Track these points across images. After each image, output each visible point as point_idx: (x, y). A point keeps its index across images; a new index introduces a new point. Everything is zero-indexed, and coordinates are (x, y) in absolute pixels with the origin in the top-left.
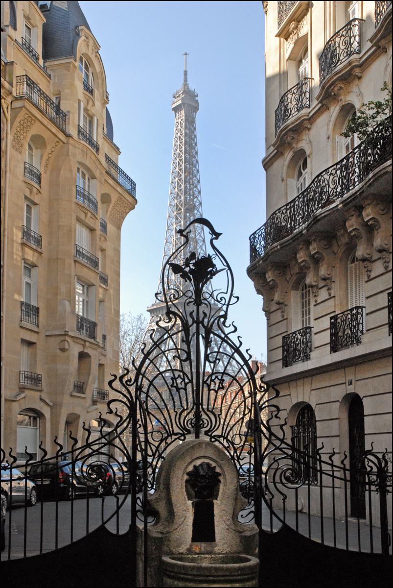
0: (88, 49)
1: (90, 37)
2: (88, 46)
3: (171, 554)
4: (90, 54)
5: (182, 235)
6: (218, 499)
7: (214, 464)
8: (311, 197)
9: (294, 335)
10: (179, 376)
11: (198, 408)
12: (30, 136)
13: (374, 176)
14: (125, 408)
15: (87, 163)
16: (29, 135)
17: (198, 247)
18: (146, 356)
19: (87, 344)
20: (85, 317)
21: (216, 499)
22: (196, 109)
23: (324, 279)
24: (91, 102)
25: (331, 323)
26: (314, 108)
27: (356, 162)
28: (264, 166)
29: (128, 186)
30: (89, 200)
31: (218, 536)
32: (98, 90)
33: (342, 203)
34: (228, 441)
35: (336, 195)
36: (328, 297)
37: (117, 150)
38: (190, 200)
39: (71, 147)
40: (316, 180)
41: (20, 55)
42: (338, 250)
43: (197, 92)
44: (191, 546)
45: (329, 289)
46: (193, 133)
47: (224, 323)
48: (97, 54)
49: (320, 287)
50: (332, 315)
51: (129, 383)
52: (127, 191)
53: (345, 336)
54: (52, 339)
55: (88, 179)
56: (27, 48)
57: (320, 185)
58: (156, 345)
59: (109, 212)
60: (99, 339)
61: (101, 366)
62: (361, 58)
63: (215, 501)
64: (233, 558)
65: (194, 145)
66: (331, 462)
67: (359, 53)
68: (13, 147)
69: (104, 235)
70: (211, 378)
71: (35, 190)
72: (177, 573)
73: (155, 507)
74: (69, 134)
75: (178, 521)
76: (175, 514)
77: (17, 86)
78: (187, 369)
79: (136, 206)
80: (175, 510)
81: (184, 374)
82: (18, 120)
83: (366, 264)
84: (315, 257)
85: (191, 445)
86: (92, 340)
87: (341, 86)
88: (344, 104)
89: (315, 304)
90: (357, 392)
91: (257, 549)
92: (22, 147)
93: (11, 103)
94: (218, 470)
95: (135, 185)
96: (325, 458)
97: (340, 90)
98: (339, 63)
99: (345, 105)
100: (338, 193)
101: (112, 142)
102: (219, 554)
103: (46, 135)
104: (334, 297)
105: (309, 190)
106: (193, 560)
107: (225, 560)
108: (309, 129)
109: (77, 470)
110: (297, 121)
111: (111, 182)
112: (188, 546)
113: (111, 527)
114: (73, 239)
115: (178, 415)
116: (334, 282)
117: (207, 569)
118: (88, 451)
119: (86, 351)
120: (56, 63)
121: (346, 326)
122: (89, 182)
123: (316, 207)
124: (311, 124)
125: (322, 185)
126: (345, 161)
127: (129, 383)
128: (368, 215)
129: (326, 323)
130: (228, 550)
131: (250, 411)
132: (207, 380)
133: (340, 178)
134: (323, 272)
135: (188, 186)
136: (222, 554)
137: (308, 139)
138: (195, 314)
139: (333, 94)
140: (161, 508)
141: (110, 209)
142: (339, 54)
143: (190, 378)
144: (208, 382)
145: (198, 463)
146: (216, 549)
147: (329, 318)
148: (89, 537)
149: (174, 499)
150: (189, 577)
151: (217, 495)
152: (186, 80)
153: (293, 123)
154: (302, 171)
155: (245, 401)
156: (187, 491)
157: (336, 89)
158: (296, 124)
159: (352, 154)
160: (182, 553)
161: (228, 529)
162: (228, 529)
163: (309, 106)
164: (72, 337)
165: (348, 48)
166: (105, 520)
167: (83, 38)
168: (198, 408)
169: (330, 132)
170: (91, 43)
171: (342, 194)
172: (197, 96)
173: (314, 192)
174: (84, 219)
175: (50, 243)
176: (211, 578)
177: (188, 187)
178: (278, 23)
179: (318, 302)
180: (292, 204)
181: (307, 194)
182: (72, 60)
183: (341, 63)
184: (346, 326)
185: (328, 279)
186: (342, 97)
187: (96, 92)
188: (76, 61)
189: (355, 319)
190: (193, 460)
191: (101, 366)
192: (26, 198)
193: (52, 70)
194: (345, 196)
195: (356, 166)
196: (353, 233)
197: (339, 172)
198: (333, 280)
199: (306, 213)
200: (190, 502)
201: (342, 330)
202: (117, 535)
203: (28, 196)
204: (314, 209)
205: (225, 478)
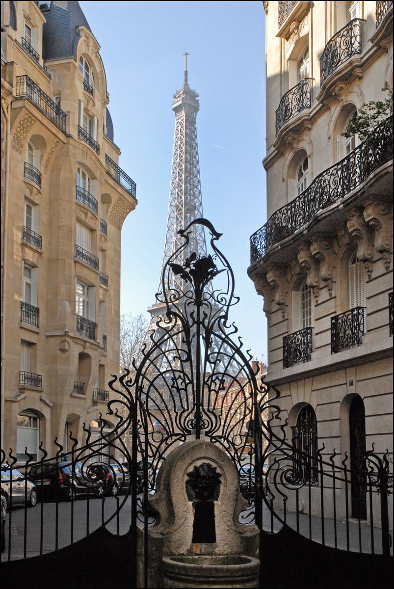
0: (89, 49)
1: (90, 37)
2: (88, 46)
3: (171, 555)
4: (90, 54)
5: (182, 235)
6: (219, 500)
7: (214, 465)
8: (312, 197)
9: (295, 336)
10: (180, 377)
11: (198, 409)
12: (30, 136)
13: (375, 176)
14: (126, 408)
15: (88, 163)
16: (29, 135)
17: (199, 248)
18: (147, 357)
19: (88, 344)
20: (85, 317)
21: (217, 500)
23: (325, 280)
24: (91, 102)
26: (315, 108)
28: (265, 167)
29: (128, 187)
30: (89, 200)
31: (218, 537)
32: (98, 90)
34: (228, 441)
36: (329, 297)
37: (117, 150)
38: (190, 200)
39: (71, 147)
40: (317, 181)
41: (20, 55)
42: (339, 251)
43: (197, 92)
44: (191, 547)
45: (330, 290)
46: (194, 133)
47: (225, 323)
49: (320, 287)
50: (333, 315)
51: (129, 384)
52: (127, 191)
53: (346, 337)
54: (52, 340)
55: (89, 179)
56: (27, 48)
57: (321, 185)
58: (157, 345)
59: (109, 212)
60: (100, 340)
61: (101, 366)
62: (362, 58)
63: (215, 502)
64: (233, 559)
65: (194, 145)
67: (360, 53)
68: (13, 147)
69: (104, 235)
70: (212, 379)
71: (35, 191)
72: (177, 574)
73: (156, 508)
74: (70, 134)
75: (178, 521)
76: (176, 515)
78: (187, 370)
79: (136, 206)
80: (176, 511)
81: (185, 374)
82: (18, 120)
83: (367, 265)
84: (316, 257)
85: (192, 446)
86: (92, 341)
87: (342, 86)
88: (344, 104)
90: (357, 393)
92: (22, 147)
93: (11, 103)
94: (218, 471)
95: (136, 185)
97: (340, 90)
98: (340, 63)
99: (346, 105)
100: (338, 194)
101: (112, 142)
102: (220, 555)
103: (46, 135)
104: (335, 297)
105: (310, 191)
106: (194, 561)
107: (228, 560)
108: (310, 129)
110: (298, 121)
111: (111, 182)
112: (189, 547)
113: (111, 528)
114: (73, 240)
115: (179, 415)
116: (335, 282)
117: (207, 569)
118: (88, 452)
119: (86, 352)
120: (56, 63)
121: (347, 326)
122: (89, 182)
123: (317, 207)
124: (312, 125)
125: (323, 186)
127: (129, 384)
128: (369, 216)
129: (327, 323)
130: (229, 551)
131: (251, 412)
132: (208, 380)
135: (189, 186)
136: (223, 555)
138: (195, 315)
139: (334, 94)
141: (110, 209)
142: (340, 54)
143: (190, 379)
144: (209, 383)
145: (199, 463)
146: (217, 550)
147: (330, 319)
148: (90, 537)
149: (174, 499)
150: (190, 578)
151: (218, 496)
152: (186, 80)
153: (294, 123)
154: (303, 171)
156: (187, 492)
157: (337, 89)
158: (296, 124)
159: (353, 154)
160: (182, 554)
161: (228, 530)
162: (228, 530)
163: (310, 106)
164: (73, 338)
165: (349, 48)
166: (105, 520)
167: (83, 38)
169: (331, 133)
170: (91, 43)
171: (343, 194)
172: (198, 96)
173: (315, 193)
175: (50, 244)
176: (212, 579)
177: (189, 188)
178: (279, 23)
179: (319, 302)
180: (293, 205)
181: (308, 194)
182: (72, 60)
184: (347, 326)
185: (329, 279)
186: (343, 97)
187: (96, 92)
188: (76, 61)
189: (356, 320)
190: (194, 461)
191: (101, 366)
192: (26, 198)
193: (52, 70)
194: (346, 196)
195: (356, 166)
196: (354, 233)
198: (334, 281)
199: (307, 213)
200: (191, 503)
201: (343, 330)
202: (117, 536)
203: (28, 196)
204: (314, 209)
205: (225, 479)
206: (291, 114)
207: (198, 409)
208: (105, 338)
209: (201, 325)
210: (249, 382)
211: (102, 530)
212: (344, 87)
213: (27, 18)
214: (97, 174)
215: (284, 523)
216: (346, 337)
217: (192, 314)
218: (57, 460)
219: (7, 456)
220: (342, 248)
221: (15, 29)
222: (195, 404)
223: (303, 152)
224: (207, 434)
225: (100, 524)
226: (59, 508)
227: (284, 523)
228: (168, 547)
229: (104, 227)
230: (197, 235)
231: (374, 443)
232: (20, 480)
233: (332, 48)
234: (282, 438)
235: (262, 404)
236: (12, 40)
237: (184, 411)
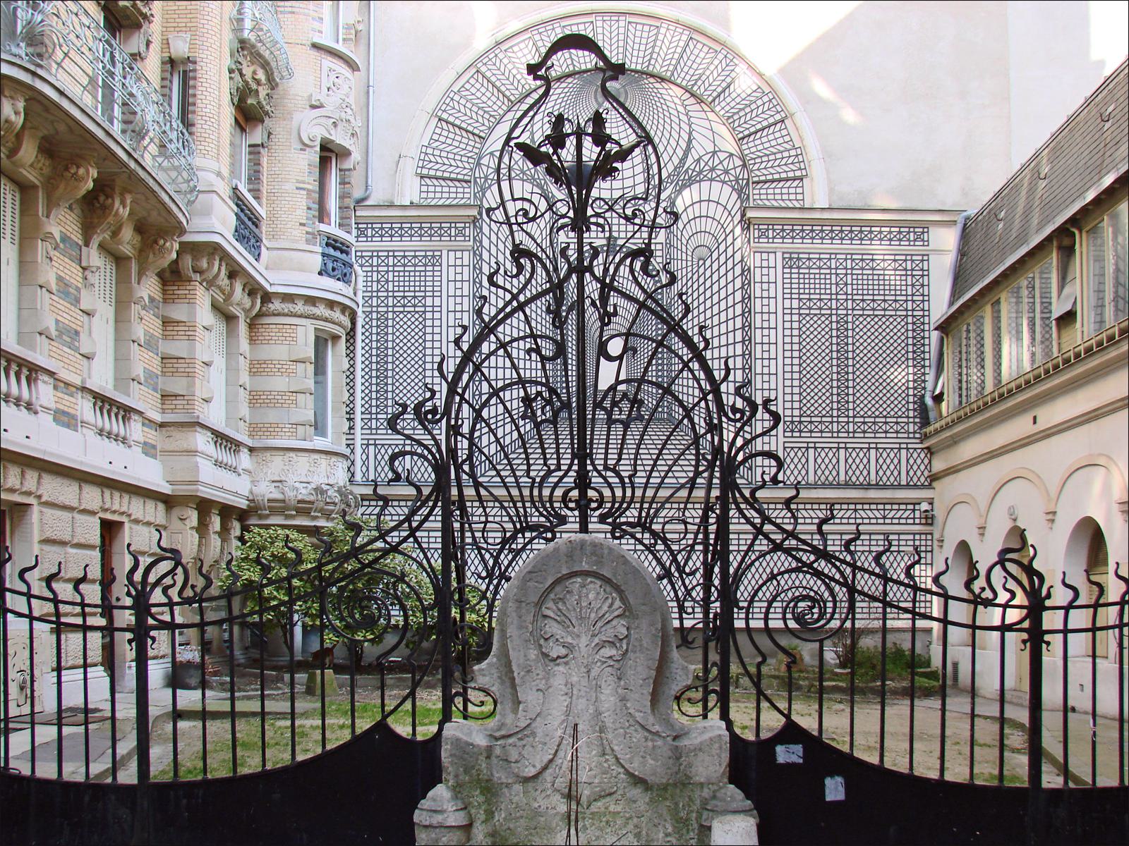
11: (582, 465)
207: (582, 465)
209: (587, 275)
210: (704, 398)
211: (381, 727)
215: (788, 717)
217: (564, 252)
219: (192, 573)
222: (574, 456)
224: (602, 519)
225: (379, 718)
227: (788, 717)
231: (87, 566)
232: (219, 623)
234: (79, 601)
235: (726, 449)
237: (549, 473)
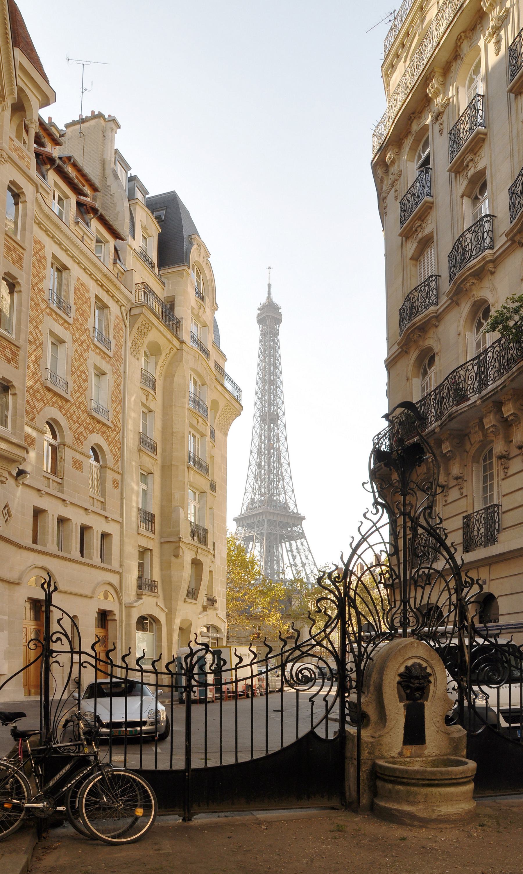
0: (200, 257)
1: (201, 245)
2: (200, 254)
3: (383, 757)
4: (201, 262)
6: (429, 700)
7: (424, 664)
8: (445, 394)
9: (422, 536)
10: (387, 572)
11: (405, 606)
12: (147, 342)
13: (519, 369)
14: (333, 605)
15: (199, 370)
16: (146, 342)
17: (282, 457)
19: (200, 550)
20: (197, 523)
21: (427, 701)
22: (279, 321)
23: (457, 478)
24: (202, 309)
25: (464, 523)
26: (443, 305)
27: (495, 356)
28: (387, 366)
29: (235, 393)
30: (200, 406)
31: (428, 739)
32: (208, 297)
33: (481, 398)
35: (473, 391)
36: (460, 496)
37: (223, 356)
38: (274, 411)
39: (184, 353)
40: (450, 377)
41: (138, 264)
42: (470, 448)
43: (280, 305)
44: (402, 749)
45: (461, 488)
46: (277, 345)
48: (208, 263)
49: (450, 486)
50: (465, 514)
51: (337, 580)
52: (234, 397)
53: (480, 536)
54: (166, 546)
55: (199, 386)
56: (143, 255)
57: (456, 381)
58: (364, 539)
59: (217, 418)
60: (210, 546)
61: (211, 572)
62: (494, 253)
63: (425, 703)
64: (444, 760)
65: (277, 356)
66: (124, 665)
67: (491, 247)
68: (131, 353)
69: (213, 441)
70: (418, 573)
71: (150, 397)
72: (399, 777)
73: (365, 710)
74: (183, 340)
75: (390, 724)
76: (387, 717)
77: (136, 293)
79: (242, 412)
80: (387, 713)
82: (136, 326)
83: (504, 462)
84: (448, 455)
85: (403, 645)
86: (204, 547)
87: (473, 281)
88: (476, 299)
89: (444, 503)
90: (491, 592)
91: (465, 750)
92: (139, 353)
93: (130, 310)
94: (429, 670)
95: (241, 391)
96: (118, 662)
97: (472, 285)
98: (472, 258)
99: (477, 301)
100: (475, 389)
101: (219, 349)
102: (429, 756)
103: (162, 341)
104: (466, 496)
105: (441, 388)
106: (405, 763)
107: (436, 763)
108: (436, 327)
109: (287, 674)
110: (425, 318)
111: (220, 388)
112: (399, 750)
113: (320, 732)
114: (186, 448)
115: (386, 613)
116: (466, 481)
117: (417, 772)
118: (297, 653)
119: (198, 558)
120: (170, 270)
121: (481, 524)
122: (199, 388)
123: (451, 404)
124: (439, 322)
125: (458, 382)
126: (483, 356)
127: (337, 580)
128: (508, 411)
129: (458, 522)
130: (437, 752)
131: (456, 608)
133: (477, 373)
134: (455, 470)
135: (272, 396)
136: (432, 756)
137: (435, 337)
139: (465, 289)
140: (371, 710)
141: (218, 415)
142: (471, 249)
143: (397, 573)
145: (410, 663)
146: (426, 752)
147: (462, 518)
148: (299, 742)
149: (386, 702)
150: (413, 781)
151: (428, 695)
152: (269, 292)
153: (421, 320)
154: (428, 370)
155: (450, 598)
156: (399, 692)
157: (468, 284)
158: (423, 321)
159: (491, 348)
160: (393, 757)
161: (438, 732)
162: (438, 732)
163: (437, 302)
164: (187, 544)
165: (481, 243)
166: (314, 725)
167: (195, 246)
168: (405, 606)
169: (461, 328)
170: (202, 251)
171: (480, 390)
172: (280, 309)
173: (448, 389)
174: (196, 426)
175: (164, 450)
176: (436, 782)
177: (272, 398)
178: (401, 223)
179: (448, 502)
180: (422, 402)
181: (440, 391)
182: (186, 268)
183: (474, 259)
184: (481, 524)
185: (460, 478)
186: (474, 293)
187: (206, 298)
188: (189, 268)
189: (491, 517)
190: (404, 662)
191: (211, 572)
192: (143, 404)
193: (166, 278)
194: (484, 393)
195: (495, 361)
196: (491, 430)
197: (476, 368)
198: (465, 479)
199: (439, 411)
200: (402, 705)
201: (476, 529)
202: (326, 741)
203: (145, 402)
204: (448, 406)
205: (436, 679)
206: (418, 311)
208: (214, 543)
212: (475, 282)
213: (144, 228)
214: (208, 381)
216: (480, 536)
218: (267, 661)
220: (474, 445)
221: (134, 238)
223: (430, 349)
226: (124, 716)
228: (379, 751)
229: (212, 433)
230: (280, 445)
233: (463, 244)
236: (132, 249)
